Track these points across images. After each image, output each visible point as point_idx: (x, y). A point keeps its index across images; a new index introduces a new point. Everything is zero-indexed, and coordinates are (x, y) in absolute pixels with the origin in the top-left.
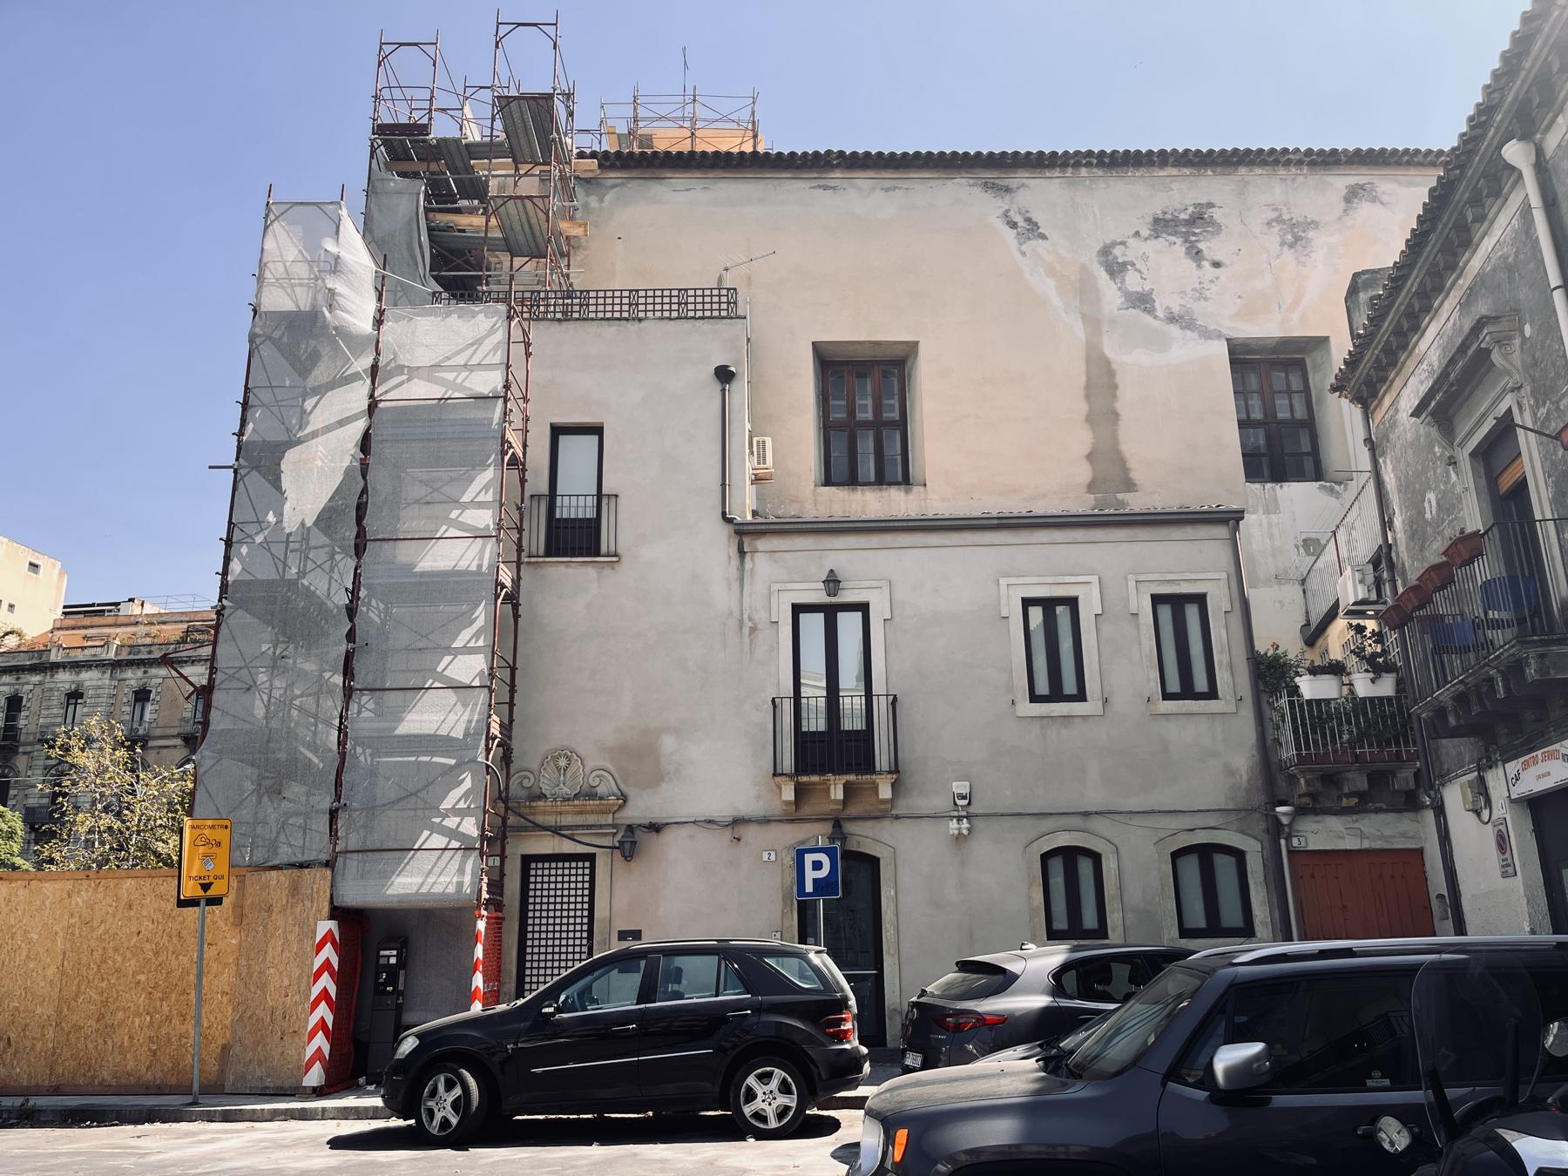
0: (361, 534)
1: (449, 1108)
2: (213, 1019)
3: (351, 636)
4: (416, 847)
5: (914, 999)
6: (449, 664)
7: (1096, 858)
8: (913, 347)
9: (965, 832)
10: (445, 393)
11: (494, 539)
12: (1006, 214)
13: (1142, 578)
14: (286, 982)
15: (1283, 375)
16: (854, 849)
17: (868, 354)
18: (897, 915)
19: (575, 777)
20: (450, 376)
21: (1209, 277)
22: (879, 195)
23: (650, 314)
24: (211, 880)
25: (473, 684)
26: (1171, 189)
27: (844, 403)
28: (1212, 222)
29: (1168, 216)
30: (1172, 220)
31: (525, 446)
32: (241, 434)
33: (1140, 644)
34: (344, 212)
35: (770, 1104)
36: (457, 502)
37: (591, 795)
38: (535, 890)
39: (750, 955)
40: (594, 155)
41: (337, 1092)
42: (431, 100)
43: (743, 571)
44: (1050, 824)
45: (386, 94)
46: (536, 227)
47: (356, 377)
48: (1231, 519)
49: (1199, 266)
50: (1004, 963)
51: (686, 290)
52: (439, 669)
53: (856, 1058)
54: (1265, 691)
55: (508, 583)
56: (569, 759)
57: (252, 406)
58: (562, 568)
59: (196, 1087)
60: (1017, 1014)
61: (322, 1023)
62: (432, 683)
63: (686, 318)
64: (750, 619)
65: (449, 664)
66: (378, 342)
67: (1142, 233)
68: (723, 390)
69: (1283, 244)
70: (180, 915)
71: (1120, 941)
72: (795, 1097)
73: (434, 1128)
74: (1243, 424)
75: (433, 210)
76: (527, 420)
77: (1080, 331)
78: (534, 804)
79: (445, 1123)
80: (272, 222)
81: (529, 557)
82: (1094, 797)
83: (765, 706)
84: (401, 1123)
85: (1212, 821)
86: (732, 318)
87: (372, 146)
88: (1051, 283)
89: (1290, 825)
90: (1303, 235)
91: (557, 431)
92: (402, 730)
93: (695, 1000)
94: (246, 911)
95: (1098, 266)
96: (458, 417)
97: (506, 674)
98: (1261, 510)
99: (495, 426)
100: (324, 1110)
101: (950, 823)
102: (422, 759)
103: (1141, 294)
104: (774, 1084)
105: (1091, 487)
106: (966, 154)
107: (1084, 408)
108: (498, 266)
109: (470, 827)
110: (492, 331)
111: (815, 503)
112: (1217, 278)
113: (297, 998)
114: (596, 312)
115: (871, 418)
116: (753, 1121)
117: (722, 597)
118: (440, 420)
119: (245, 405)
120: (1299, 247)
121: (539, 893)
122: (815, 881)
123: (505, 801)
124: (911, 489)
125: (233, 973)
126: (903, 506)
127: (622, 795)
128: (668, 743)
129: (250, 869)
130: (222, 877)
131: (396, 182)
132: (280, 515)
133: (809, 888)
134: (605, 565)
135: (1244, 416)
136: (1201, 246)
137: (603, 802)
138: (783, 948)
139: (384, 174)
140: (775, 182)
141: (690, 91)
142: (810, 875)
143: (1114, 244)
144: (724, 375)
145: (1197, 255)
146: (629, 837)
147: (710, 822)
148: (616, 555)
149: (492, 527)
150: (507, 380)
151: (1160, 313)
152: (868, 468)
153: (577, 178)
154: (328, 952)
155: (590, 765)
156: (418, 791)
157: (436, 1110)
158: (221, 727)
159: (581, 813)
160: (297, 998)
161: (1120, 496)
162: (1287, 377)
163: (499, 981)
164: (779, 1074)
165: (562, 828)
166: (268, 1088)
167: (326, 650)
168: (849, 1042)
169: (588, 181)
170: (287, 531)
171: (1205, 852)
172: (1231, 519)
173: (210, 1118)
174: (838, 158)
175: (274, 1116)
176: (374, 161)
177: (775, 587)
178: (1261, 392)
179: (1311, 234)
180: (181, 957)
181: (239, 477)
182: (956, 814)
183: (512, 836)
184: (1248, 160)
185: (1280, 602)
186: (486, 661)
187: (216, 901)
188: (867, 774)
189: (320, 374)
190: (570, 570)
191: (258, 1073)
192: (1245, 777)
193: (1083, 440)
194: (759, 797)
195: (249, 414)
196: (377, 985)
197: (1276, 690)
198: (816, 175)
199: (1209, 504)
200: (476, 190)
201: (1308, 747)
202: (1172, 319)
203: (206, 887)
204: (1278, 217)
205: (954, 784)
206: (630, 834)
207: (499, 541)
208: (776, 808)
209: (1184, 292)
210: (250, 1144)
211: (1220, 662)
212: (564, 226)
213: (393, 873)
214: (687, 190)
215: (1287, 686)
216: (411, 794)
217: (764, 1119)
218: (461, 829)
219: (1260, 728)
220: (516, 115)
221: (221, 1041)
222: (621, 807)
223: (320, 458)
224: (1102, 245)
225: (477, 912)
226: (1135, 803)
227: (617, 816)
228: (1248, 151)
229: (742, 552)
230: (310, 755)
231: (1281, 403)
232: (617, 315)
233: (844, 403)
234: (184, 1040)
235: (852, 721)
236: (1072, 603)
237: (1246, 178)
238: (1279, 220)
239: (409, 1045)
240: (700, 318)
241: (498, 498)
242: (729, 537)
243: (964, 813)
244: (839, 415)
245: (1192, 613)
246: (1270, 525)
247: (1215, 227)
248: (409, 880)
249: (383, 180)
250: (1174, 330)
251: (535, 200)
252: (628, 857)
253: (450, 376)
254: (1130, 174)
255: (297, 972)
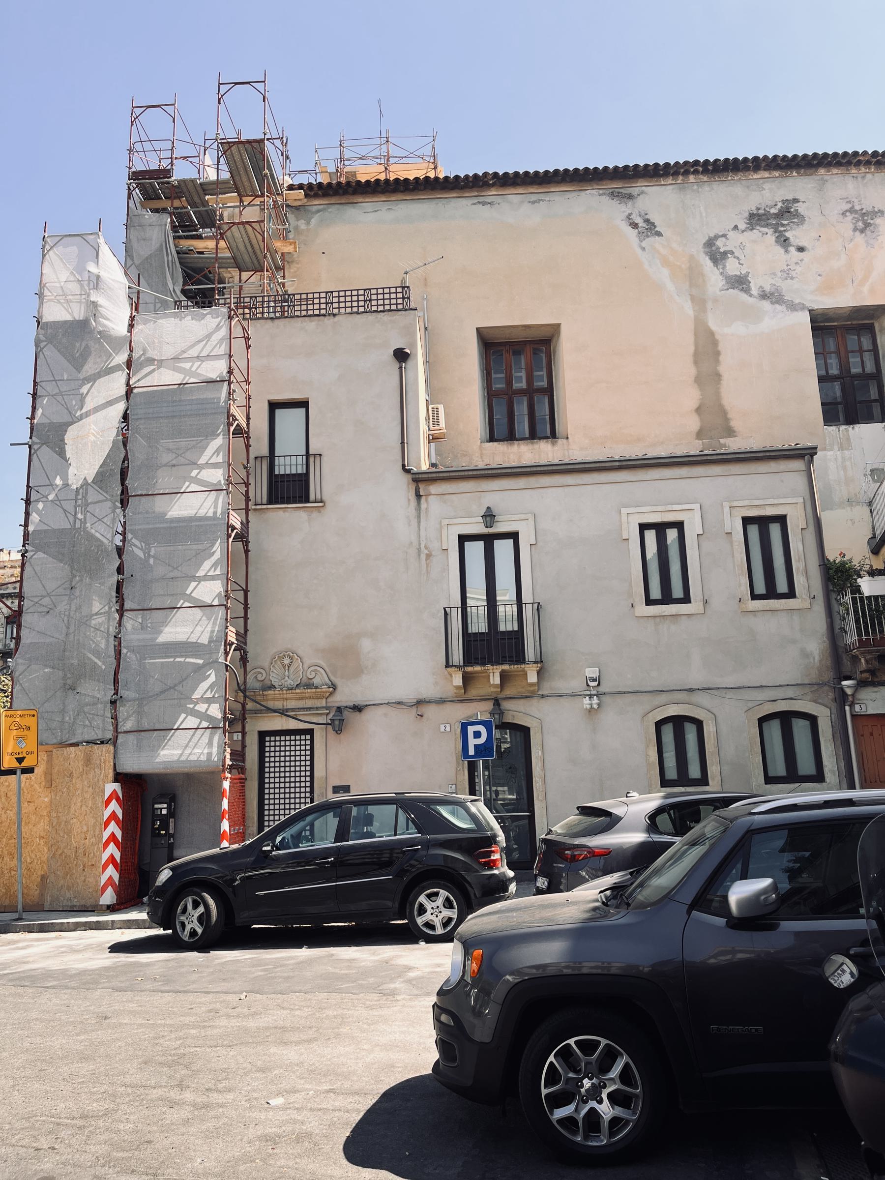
0: (124, 491)
1: (196, 921)
2: (33, 856)
3: (120, 570)
4: (175, 727)
5: (543, 836)
6: (195, 589)
7: (699, 724)
8: (556, 328)
9: (595, 706)
10: (184, 379)
11: (225, 492)
12: (629, 217)
13: (735, 504)
14: (85, 828)
15: (856, 337)
16: (510, 721)
17: (521, 336)
18: (544, 770)
19: (296, 671)
20: (187, 365)
21: (794, 260)
22: (526, 208)
23: (342, 310)
24: (24, 755)
25: (214, 603)
26: (763, 189)
27: (503, 375)
28: (797, 214)
29: (761, 211)
30: (764, 215)
31: (248, 418)
32: (32, 418)
33: (733, 557)
34: (101, 241)
35: (437, 916)
36: (195, 464)
37: (309, 685)
38: (270, 757)
39: (421, 804)
40: (301, 187)
41: (126, 908)
42: (172, 150)
43: (420, 510)
44: (663, 698)
45: (138, 147)
46: (256, 247)
47: (117, 368)
48: (806, 454)
49: (787, 251)
50: (611, 808)
51: (370, 290)
52: (188, 592)
53: (503, 881)
54: (833, 591)
55: (238, 525)
56: (291, 658)
57: (40, 396)
58: (281, 512)
59: (20, 907)
60: (624, 847)
61: (112, 858)
62: (183, 604)
63: (369, 312)
64: (426, 548)
65: (195, 589)
66: (131, 341)
67: (740, 227)
68: (401, 368)
69: (855, 229)
70: (6, 781)
71: (719, 789)
72: (456, 910)
73: (185, 936)
74: (822, 379)
75: (180, 237)
76: (249, 398)
77: (689, 309)
78: (265, 693)
79: (193, 933)
80: (48, 251)
81: (256, 505)
82: (696, 676)
83: (440, 614)
84: (161, 931)
85: (790, 693)
86: (406, 310)
87: (129, 189)
88: (665, 272)
89: (853, 695)
90: (872, 222)
91: (274, 406)
92: (162, 638)
93: (384, 839)
94: (55, 777)
95: (704, 256)
96: (202, 397)
97: (240, 596)
98: (836, 447)
99: (222, 403)
100: (113, 922)
101: (584, 700)
102: (178, 660)
103: (740, 277)
104: (440, 901)
105: (700, 435)
106: (596, 169)
107: (693, 371)
108: (231, 280)
109: (216, 711)
110: (218, 328)
111: (482, 455)
112: (801, 260)
113: (93, 840)
114: (301, 310)
115: (525, 387)
116: (424, 929)
117: (404, 531)
118: (180, 401)
119: (34, 395)
120: (868, 232)
121: (272, 759)
122: (476, 746)
123: (244, 691)
124: (556, 442)
125: (47, 823)
126: (550, 456)
127: (332, 684)
128: (366, 644)
129: (55, 746)
130: (32, 753)
131: (148, 215)
132: (65, 478)
133: (472, 752)
134: (314, 509)
135: (823, 373)
136: (787, 234)
137: (318, 690)
138: (446, 798)
139: (140, 211)
140: (444, 201)
141: (384, 134)
142: (472, 742)
143: (717, 237)
144: (401, 356)
145: (784, 242)
146: (338, 716)
147: (399, 703)
148: (321, 502)
149: (223, 482)
150: (230, 368)
151: (754, 291)
152: (523, 426)
153: (288, 206)
154: (114, 806)
155: (307, 662)
156: (175, 685)
157: (186, 923)
158: (28, 641)
159: (302, 699)
160: (93, 840)
161: (722, 441)
162: (859, 339)
163: (244, 825)
164: (443, 893)
165: (287, 710)
166: (75, 906)
167: (103, 580)
168: (497, 868)
169: (297, 208)
170: (74, 487)
171: (786, 718)
172: (806, 454)
173: (30, 929)
174: (493, 178)
175: (76, 927)
176: (131, 201)
177: (446, 522)
178: (838, 352)
179: (878, 221)
180: (8, 812)
181: (33, 451)
182: (588, 693)
183: (251, 718)
184: (826, 162)
185: (851, 520)
186: (223, 586)
187: (29, 770)
188: (517, 664)
189: (90, 368)
190: (287, 514)
191: (68, 895)
192: (817, 658)
193: (691, 397)
194: (436, 683)
195: (38, 402)
196: (153, 829)
197: (843, 589)
198: (476, 194)
199: (789, 442)
200: (209, 219)
201: (867, 633)
202: (764, 296)
203: (20, 760)
204: (851, 208)
205: (587, 669)
206: (339, 714)
207: (228, 493)
208: (450, 692)
209: (774, 274)
210: (53, 950)
211: (798, 569)
212: (278, 245)
213: (160, 746)
214: (376, 211)
215: (852, 586)
216: (170, 688)
217: (433, 927)
218: (208, 713)
219: (829, 620)
220: (237, 158)
221: (40, 873)
222: (331, 694)
223: (93, 435)
224: (707, 238)
225: (222, 775)
226: (730, 680)
227: (329, 700)
228: (826, 155)
229: (418, 496)
230: (96, 660)
231: (854, 360)
232: (317, 312)
233: (503, 375)
234: (13, 873)
235: (507, 623)
236: (679, 526)
237: (826, 177)
238: (852, 210)
239: (165, 875)
240: (381, 311)
241: (227, 460)
242: (408, 484)
243: (595, 692)
244: (499, 386)
245: (775, 530)
246: (844, 459)
247: (800, 218)
248: (172, 752)
249: (139, 215)
250: (766, 305)
251: (253, 225)
252: (339, 731)
253: (187, 365)
254: (730, 178)
255: (92, 821)
